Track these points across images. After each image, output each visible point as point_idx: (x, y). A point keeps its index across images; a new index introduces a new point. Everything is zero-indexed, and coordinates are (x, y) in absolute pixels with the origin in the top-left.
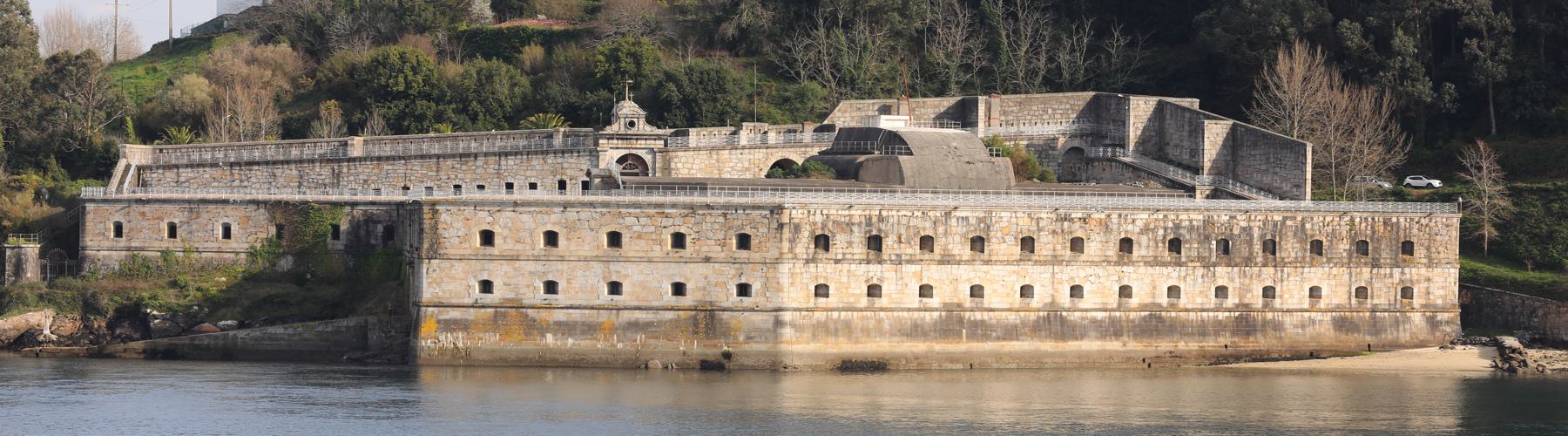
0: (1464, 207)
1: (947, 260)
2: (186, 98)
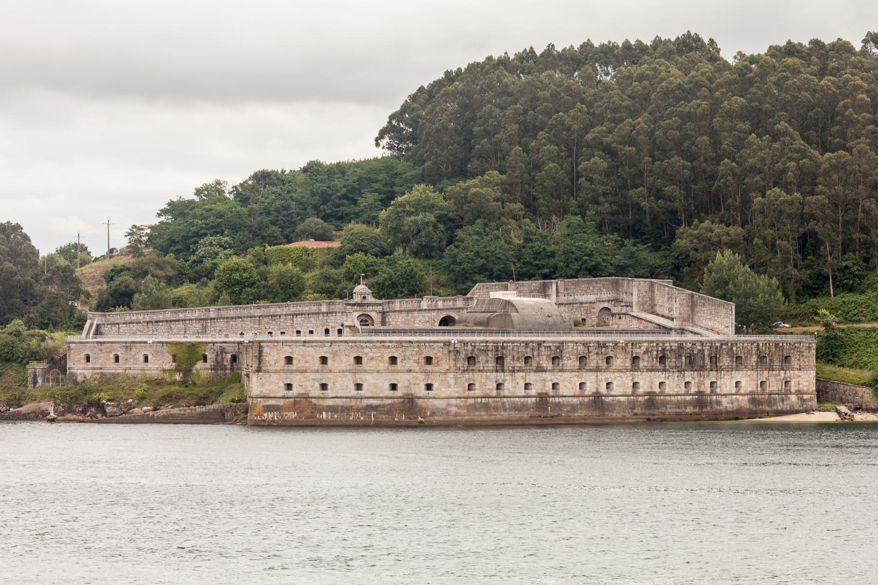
1: (540, 369)
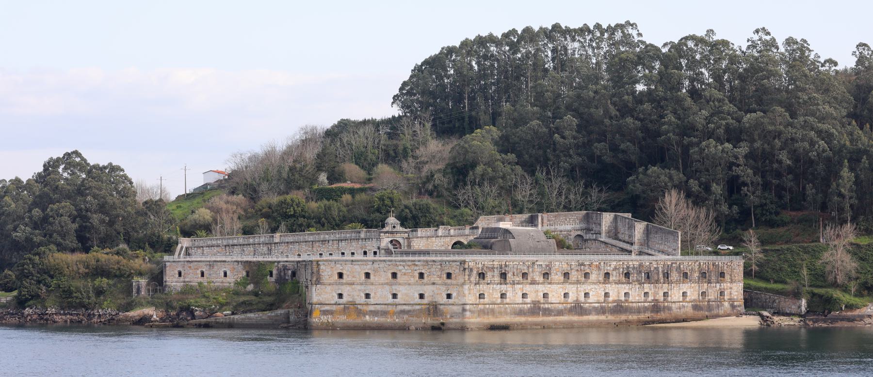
0: (744, 258)
1: (533, 282)
2: (201, 218)
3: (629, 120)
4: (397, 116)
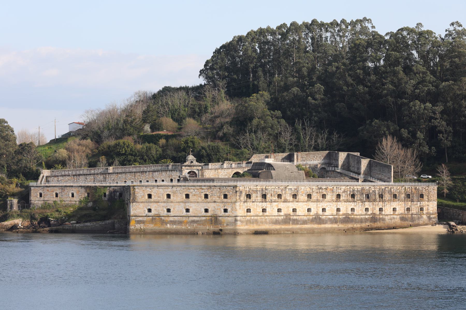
0: (438, 184)
1: (286, 201)
2: (60, 156)
3: (361, 87)
4: (203, 84)
